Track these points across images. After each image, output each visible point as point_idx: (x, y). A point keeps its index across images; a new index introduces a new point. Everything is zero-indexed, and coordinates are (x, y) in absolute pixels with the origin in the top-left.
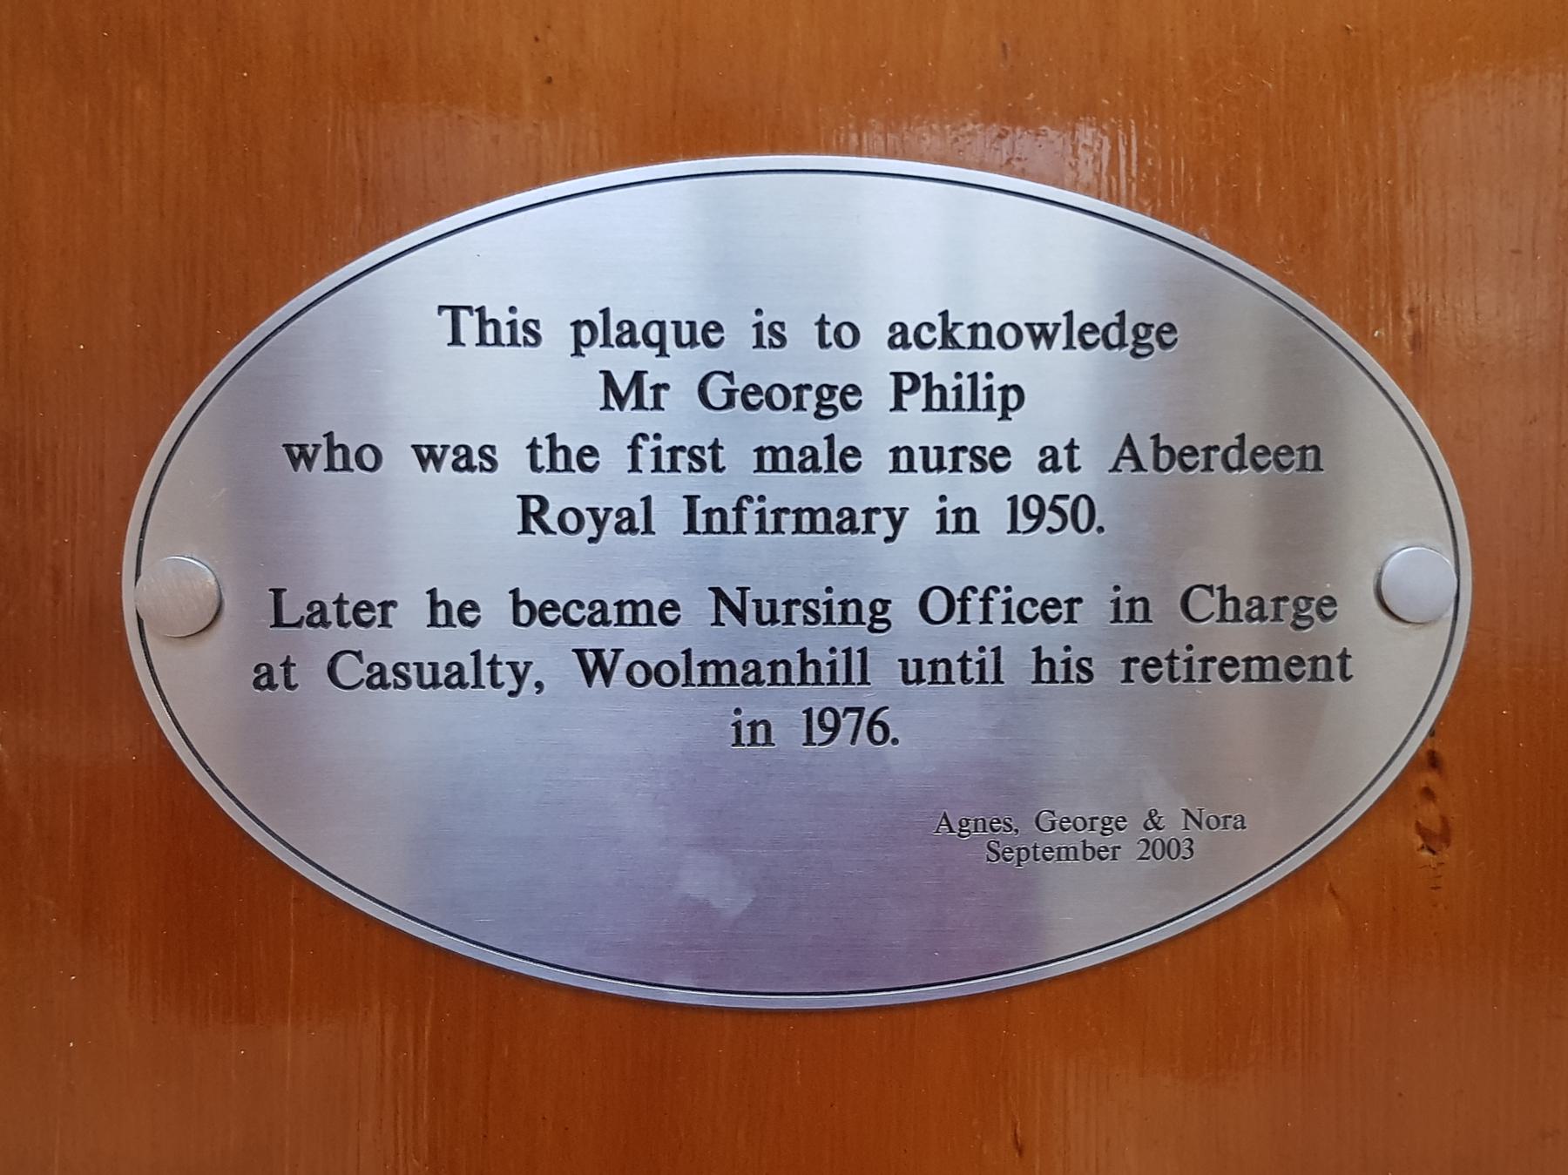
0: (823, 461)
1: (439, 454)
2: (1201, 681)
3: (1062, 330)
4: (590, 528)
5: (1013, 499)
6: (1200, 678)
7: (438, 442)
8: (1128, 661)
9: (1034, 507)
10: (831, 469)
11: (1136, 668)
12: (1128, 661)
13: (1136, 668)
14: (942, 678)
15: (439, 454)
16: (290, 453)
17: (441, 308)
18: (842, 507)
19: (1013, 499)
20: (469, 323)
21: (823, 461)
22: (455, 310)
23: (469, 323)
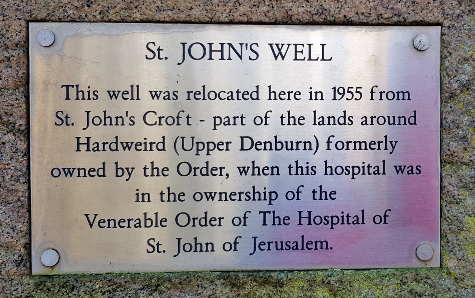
0: (300, 246)
1: (246, 170)
2: (359, 149)
3: (251, 170)
4: (126, 175)
5: (334, 88)
6: (364, 148)
7: (71, 166)
8: (189, 93)
9: (341, 91)
10: (303, 249)
11: (192, 95)
12: (189, 93)
13: (192, 95)
14: (363, 144)
15: (246, 170)
16: (240, 170)
17: (63, 86)
18: (325, 215)
19: (334, 88)
20: (73, 92)
21: (300, 246)
22: (67, 87)
23: (73, 92)
